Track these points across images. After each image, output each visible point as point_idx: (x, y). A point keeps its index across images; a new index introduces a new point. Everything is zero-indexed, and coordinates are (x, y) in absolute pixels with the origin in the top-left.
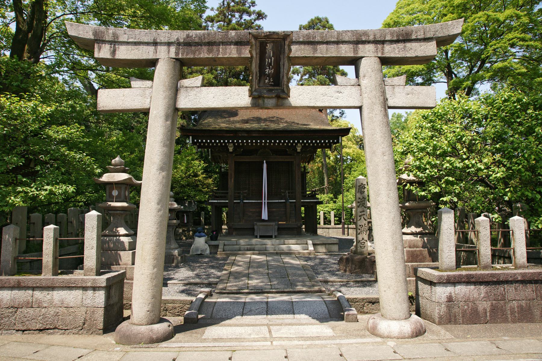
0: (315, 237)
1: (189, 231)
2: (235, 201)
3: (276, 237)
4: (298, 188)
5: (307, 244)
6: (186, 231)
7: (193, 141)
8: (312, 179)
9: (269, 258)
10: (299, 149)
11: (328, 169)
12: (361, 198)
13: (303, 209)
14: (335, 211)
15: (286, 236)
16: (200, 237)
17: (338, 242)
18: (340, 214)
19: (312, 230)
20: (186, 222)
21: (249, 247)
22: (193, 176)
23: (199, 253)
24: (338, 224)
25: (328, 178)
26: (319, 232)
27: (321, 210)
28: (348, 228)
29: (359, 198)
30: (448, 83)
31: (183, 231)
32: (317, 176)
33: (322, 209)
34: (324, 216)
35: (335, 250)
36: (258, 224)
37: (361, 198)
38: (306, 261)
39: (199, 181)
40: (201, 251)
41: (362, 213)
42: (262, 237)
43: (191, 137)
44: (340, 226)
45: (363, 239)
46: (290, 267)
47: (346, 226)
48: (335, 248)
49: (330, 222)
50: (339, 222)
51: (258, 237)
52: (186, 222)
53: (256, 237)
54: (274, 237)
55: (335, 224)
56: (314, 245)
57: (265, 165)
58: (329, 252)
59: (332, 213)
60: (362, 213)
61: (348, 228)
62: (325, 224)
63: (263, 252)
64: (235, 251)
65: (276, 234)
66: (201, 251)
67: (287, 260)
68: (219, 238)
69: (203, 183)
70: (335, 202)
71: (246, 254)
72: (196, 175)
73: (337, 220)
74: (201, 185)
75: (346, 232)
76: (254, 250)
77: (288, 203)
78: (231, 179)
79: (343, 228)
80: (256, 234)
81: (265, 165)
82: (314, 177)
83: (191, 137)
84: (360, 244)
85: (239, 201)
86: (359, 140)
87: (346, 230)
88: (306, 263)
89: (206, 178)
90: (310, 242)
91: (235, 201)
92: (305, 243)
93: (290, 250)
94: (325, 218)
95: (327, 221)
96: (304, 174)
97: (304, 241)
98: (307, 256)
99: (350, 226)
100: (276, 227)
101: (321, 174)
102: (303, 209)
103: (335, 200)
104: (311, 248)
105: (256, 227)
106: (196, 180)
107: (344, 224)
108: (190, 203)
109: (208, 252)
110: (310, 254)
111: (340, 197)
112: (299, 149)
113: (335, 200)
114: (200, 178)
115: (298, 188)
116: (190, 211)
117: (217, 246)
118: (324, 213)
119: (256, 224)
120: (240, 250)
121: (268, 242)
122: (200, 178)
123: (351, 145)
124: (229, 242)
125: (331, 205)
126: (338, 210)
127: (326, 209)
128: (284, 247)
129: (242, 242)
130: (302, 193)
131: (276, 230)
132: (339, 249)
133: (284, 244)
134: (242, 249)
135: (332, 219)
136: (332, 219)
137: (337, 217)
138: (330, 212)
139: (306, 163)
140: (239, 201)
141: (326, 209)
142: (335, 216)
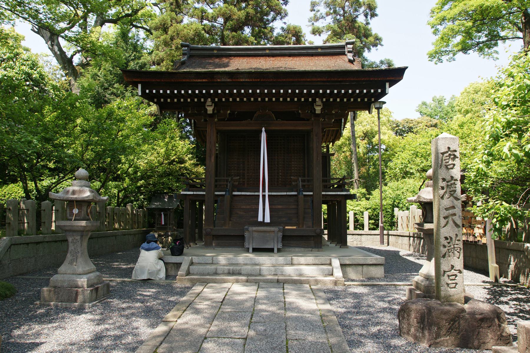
0: (343, 252)
1: (167, 236)
2: (217, 193)
3: (279, 250)
4: (317, 171)
5: (330, 264)
6: (163, 236)
7: (143, 91)
8: (337, 169)
9: (261, 293)
10: (318, 109)
11: (358, 159)
12: (448, 178)
13: (325, 207)
14: (370, 211)
15: (297, 249)
16: (148, 250)
17: (383, 262)
18: (377, 216)
19: (339, 237)
20: (163, 223)
21: (231, 268)
22: (178, 163)
23: (145, 277)
24: (374, 229)
25: (358, 170)
26: (350, 240)
27: (351, 207)
28: (388, 235)
29: (444, 180)
30: (524, 38)
31: (160, 236)
32: (343, 167)
33: (352, 208)
34: (355, 218)
35: (378, 275)
36: (251, 229)
37: (448, 178)
38: (328, 300)
39: (186, 168)
40: (150, 273)
41: (451, 212)
42: (256, 250)
43: (140, 86)
44: (377, 232)
45: (453, 267)
46: (296, 318)
47: (385, 232)
48: (379, 272)
49: (362, 226)
50: (375, 226)
51: (251, 250)
52: (163, 223)
53: (247, 251)
54: (276, 250)
55: (369, 229)
56: (343, 266)
57: (264, 136)
58: (370, 279)
59: (366, 214)
60: (451, 212)
61: (388, 235)
62: (355, 228)
63: (254, 279)
64: (208, 274)
65: (280, 246)
66: (150, 273)
67: (293, 297)
68: (185, 250)
69: (191, 171)
70: (368, 199)
71: (225, 281)
72: (182, 161)
73: (373, 224)
74: (188, 174)
75: (385, 241)
76: (240, 274)
77: (301, 196)
78: (210, 157)
79: (382, 235)
80: (246, 245)
81: (264, 136)
82: (341, 169)
83: (140, 86)
84: (446, 277)
85: (223, 193)
86: (395, 126)
87: (385, 237)
88: (328, 307)
89: (196, 165)
90: (336, 263)
91: (217, 193)
92: (328, 262)
93: (301, 275)
94: (356, 221)
95: (359, 225)
96: (326, 158)
97: (324, 259)
98: (331, 286)
99: (391, 232)
100: (280, 234)
101: (349, 164)
102: (325, 207)
103: (368, 196)
104: (338, 273)
105: (246, 234)
106: (181, 168)
107: (383, 229)
108: (170, 197)
109: (162, 275)
110: (336, 283)
111: (376, 193)
112: (318, 109)
113: (368, 196)
114: (187, 165)
115: (317, 171)
116: (169, 209)
117: (178, 265)
118: (355, 214)
119: (247, 230)
120: (216, 274)
121: (266, 262)
122: (187, 165)
123: (386, 131)
124: (201, 258)
125: (364, 203)
126: (374, 209)
127: (357, 208)
128: (289, 270)
129: (223, 259)
130: (324, 181)
131: (280, 240)
132: (385, 272)
133: (292, 264)
134: (219, 271)
135: (366, 221)
136: (366, 221)
137: (372, 219)
138: (362, 213)
139: (330, 142)
140: (223, 193)
141: (357, 208)
142: (370, 218)
